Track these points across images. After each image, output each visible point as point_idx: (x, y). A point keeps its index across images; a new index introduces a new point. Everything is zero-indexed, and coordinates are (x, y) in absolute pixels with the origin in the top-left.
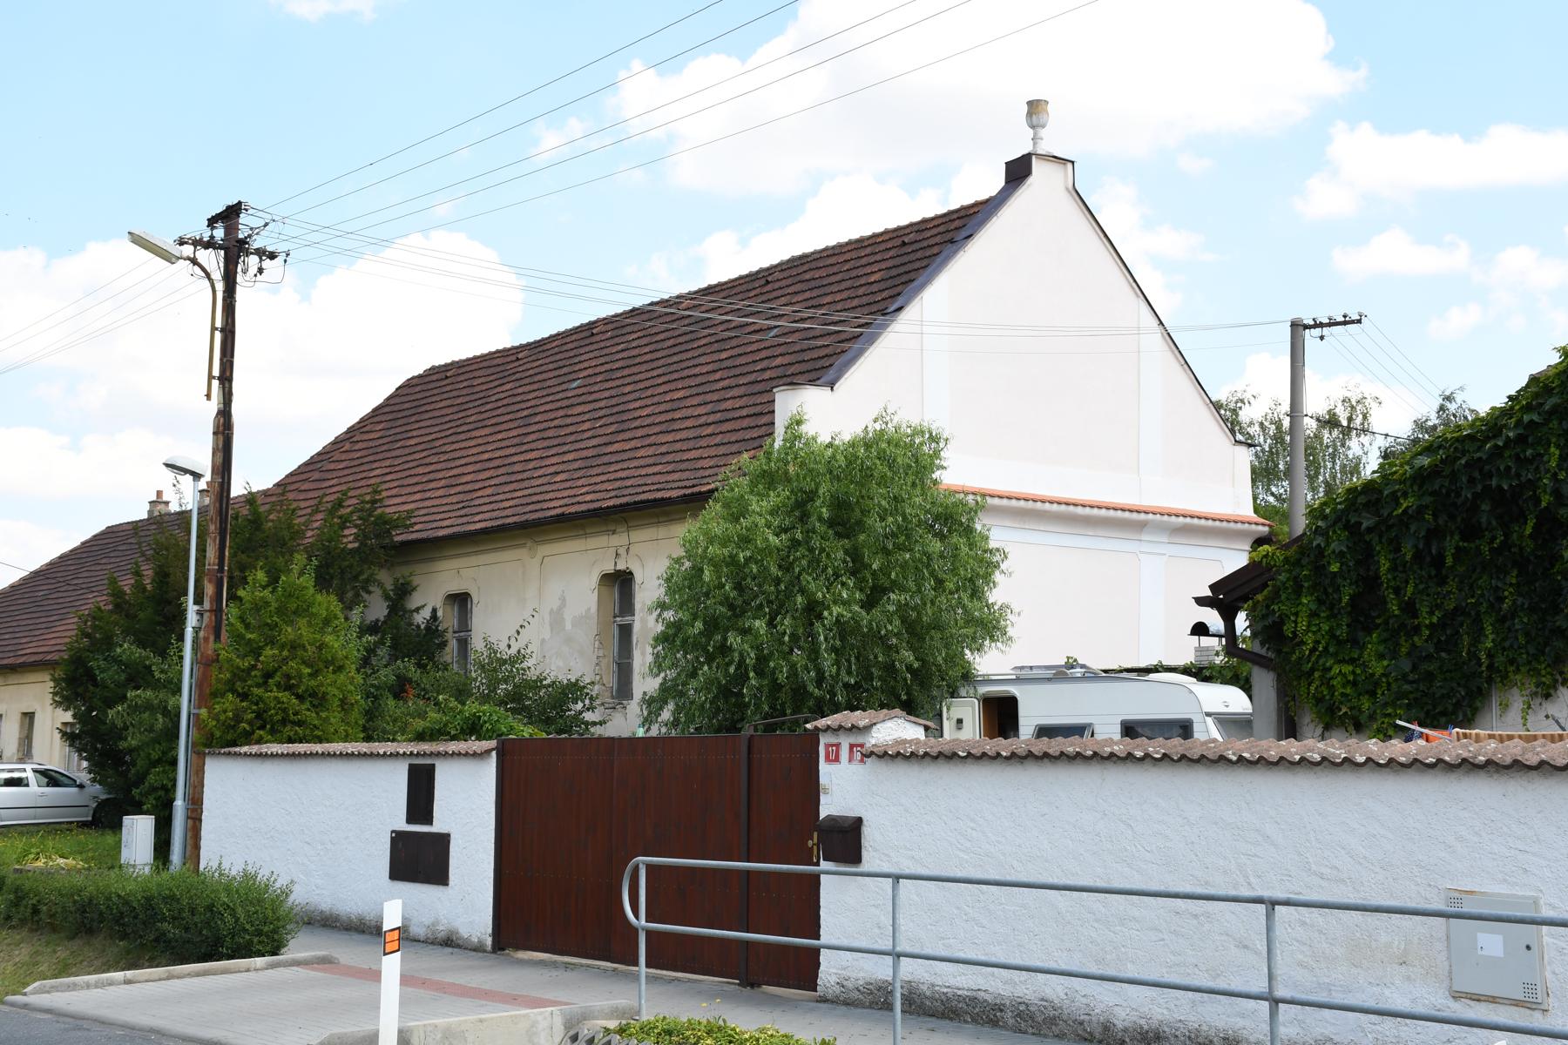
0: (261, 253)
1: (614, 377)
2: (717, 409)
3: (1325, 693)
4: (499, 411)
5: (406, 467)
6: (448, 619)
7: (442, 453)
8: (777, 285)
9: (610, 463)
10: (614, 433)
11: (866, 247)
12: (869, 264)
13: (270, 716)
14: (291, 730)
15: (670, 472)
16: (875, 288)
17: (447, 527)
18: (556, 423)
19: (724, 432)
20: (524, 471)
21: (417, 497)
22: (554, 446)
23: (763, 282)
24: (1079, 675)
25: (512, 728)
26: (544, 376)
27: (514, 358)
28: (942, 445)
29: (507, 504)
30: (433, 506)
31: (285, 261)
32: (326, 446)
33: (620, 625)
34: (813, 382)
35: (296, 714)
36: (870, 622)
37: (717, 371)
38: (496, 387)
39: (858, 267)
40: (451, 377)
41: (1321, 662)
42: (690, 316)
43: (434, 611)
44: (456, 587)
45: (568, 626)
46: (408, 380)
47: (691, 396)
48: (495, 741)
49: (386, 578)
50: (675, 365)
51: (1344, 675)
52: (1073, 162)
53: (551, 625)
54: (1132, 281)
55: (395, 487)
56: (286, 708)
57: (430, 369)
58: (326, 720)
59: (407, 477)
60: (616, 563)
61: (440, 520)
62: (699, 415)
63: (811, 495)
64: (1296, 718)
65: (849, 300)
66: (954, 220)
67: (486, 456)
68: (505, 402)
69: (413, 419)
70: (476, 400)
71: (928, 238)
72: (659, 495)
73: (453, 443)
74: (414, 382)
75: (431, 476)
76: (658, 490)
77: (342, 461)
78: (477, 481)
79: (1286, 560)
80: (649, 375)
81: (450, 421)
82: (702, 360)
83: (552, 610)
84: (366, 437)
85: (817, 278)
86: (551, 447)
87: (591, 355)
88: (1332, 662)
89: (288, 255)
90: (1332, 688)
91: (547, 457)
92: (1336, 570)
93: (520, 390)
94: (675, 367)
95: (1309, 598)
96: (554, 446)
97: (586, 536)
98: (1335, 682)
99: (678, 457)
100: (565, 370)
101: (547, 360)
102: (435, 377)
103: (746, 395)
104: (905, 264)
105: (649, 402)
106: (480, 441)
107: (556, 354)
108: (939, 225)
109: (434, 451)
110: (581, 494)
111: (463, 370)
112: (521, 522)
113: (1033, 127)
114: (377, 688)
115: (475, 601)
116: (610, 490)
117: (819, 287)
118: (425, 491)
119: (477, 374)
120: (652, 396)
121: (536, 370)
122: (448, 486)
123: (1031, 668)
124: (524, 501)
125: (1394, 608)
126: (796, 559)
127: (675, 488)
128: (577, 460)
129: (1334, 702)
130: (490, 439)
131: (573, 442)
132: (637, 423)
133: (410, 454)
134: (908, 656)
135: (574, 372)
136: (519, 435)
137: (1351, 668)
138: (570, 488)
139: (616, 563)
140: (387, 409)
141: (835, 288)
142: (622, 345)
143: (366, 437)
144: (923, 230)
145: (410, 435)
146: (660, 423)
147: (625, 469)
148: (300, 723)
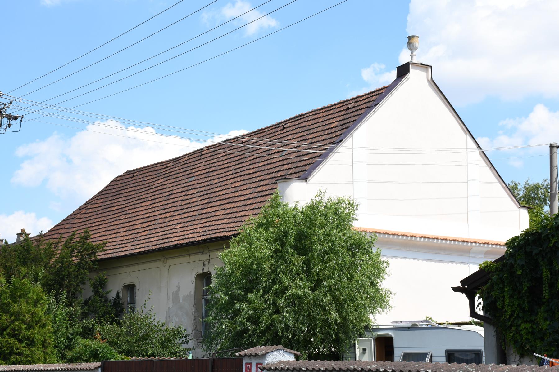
0: (10, 117)
1: (210, 175)
2: (255, 191)
3: (518, 338)
4: (155, 193)
5: (110, 221)
6: (125, 298)
7: (127, 214)
8: (288, 129)
9: (203, 219)
10: (207, 203)
11: (331, 110)
12: (332, 118)
13: (3, 351)
14: (14, 358)
15: (230, 223)
16: (333, 130)
17: (124, 251)
18: (181, 198)
19: (257, 203)
20: (163, 223)
21: (113, 236)
22: (178, 210)
23: (282, 128)
24: (424, 326)
25: (113, 356)
26: (178, 175)
27: (165, 166)
28: (355, 208)
29: (153, 239)
30: (120, 241)
31: (21, 121)
32: (75, 211)
33: (206, 300)
34: (298, 178)
35: (17, 349)
36: (313, 298)
37: (257, 172)
38: (156, 181)
39: (326, 120)
40: (135, 176)
41: (516, 321)
42: (258, 146)
43: (118, 293)
44: (128, 280)
45: (181, 301)
46: (116, 178)
47: (244, 185)
48: (100, 363)
49: (95, 277)
50: (238, 169)
51: (527, 329)
52: (431, 67)
53: (173, 299)
54: (462, 125)
55: (103, 231)
56: (12, 346)
57: (126, 172)
58: (32, 352)
59: (109, 226)
60: (203, 269)
61: (122, 248)
62: (246, 194)
63: (286, 233)
64: (506, 351)
65: (321, 137)
66: (373, 96)
67: (147, 215)
68: (159, 188)
69: (116, 197)
70: (146, 187)
71: (360, 105)
72: (222, 234)
73: (133, 209)
74: (118, 179)
75: (121, 226)
76: (223, 232)
77: (81, 218)
78: (141, 228)
79: (497, 268)
80: (226, 174)
81: (133, 198)
82: (251, 167)
83: (173, 292)
84: (93, 206)
85: (307, 126)
86: (177, 211)
87: (201, 165)
88: (521, 321)
89: (22, 118)
90: (521, 335)
91: (175, 215)
92: (520, 274)
93: (166, 182)
94: (238, 170)
95: (508, 288)
96: (178, 210)
97: (189, 254)
98: (522, 332)
99: (234, 215)
100: (188, 172)
101: (180, 168)
102: (128, 176)
103: (268, 184)
104: (348, 118)
105: (224, 188)
106: (145, 208)
107: (185, 164)
108: (365, 99)
109: (123, 213)
110: (188, 234)
111: (142, 172)
112: (158, 248)
113: (411, 49)
114: (72, 334)
115: (137, 288)
116: (201, 232)
117: (308, 130)
118: (118, 233)
119: (147, 174)
120: (226, 185)
121: (175, 173)
122: (128, 231)
123: (401, 322)
124: (161, 238)
125: (546, 294)
126: (278, 266)
127: (231, 231)
128: (189, 217)
129: (523, 343)
130: (150, 207)
131: (188, 208)
132: (217, 199)
133: (112, 215)
134: (334, 315)
135: (192, 173)
136: (163, 205)
137: (530, 325)
138: (183, 231)
139: (203, 269)
140: (104, 192)
141: (314, 131)
142: (215, 160)
143: (93, 206)
144: (358, 102)
145: (114, 205)
146: (228, 198)
147: (209, 222)
148: (20, 354)
